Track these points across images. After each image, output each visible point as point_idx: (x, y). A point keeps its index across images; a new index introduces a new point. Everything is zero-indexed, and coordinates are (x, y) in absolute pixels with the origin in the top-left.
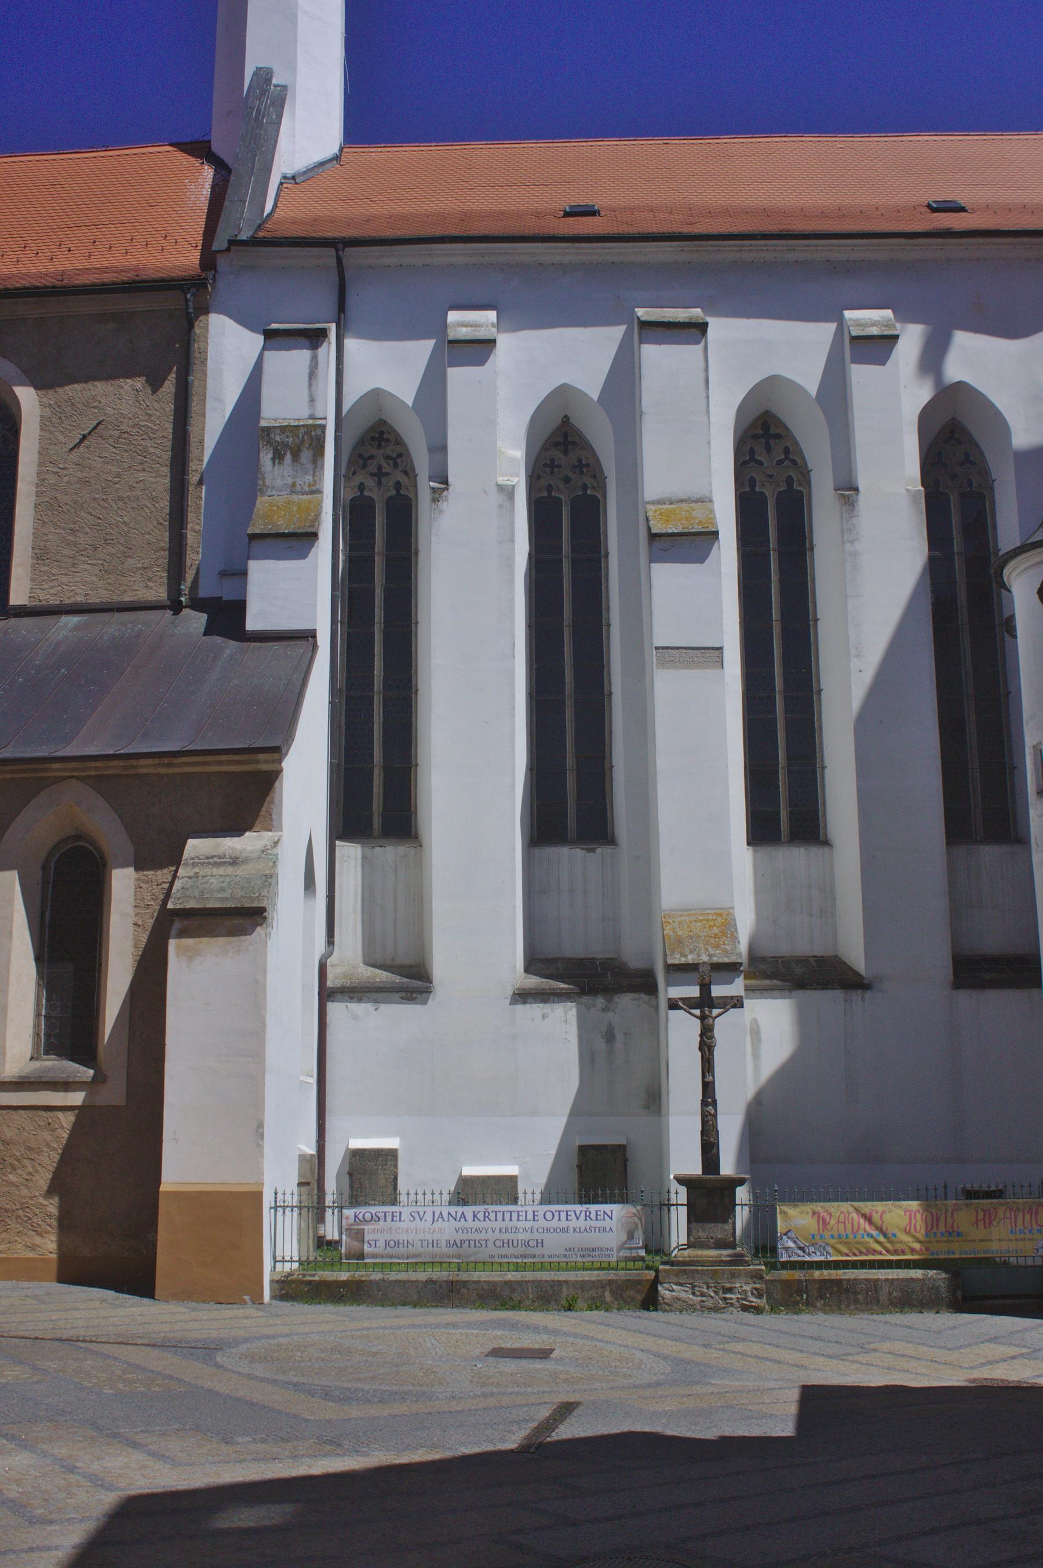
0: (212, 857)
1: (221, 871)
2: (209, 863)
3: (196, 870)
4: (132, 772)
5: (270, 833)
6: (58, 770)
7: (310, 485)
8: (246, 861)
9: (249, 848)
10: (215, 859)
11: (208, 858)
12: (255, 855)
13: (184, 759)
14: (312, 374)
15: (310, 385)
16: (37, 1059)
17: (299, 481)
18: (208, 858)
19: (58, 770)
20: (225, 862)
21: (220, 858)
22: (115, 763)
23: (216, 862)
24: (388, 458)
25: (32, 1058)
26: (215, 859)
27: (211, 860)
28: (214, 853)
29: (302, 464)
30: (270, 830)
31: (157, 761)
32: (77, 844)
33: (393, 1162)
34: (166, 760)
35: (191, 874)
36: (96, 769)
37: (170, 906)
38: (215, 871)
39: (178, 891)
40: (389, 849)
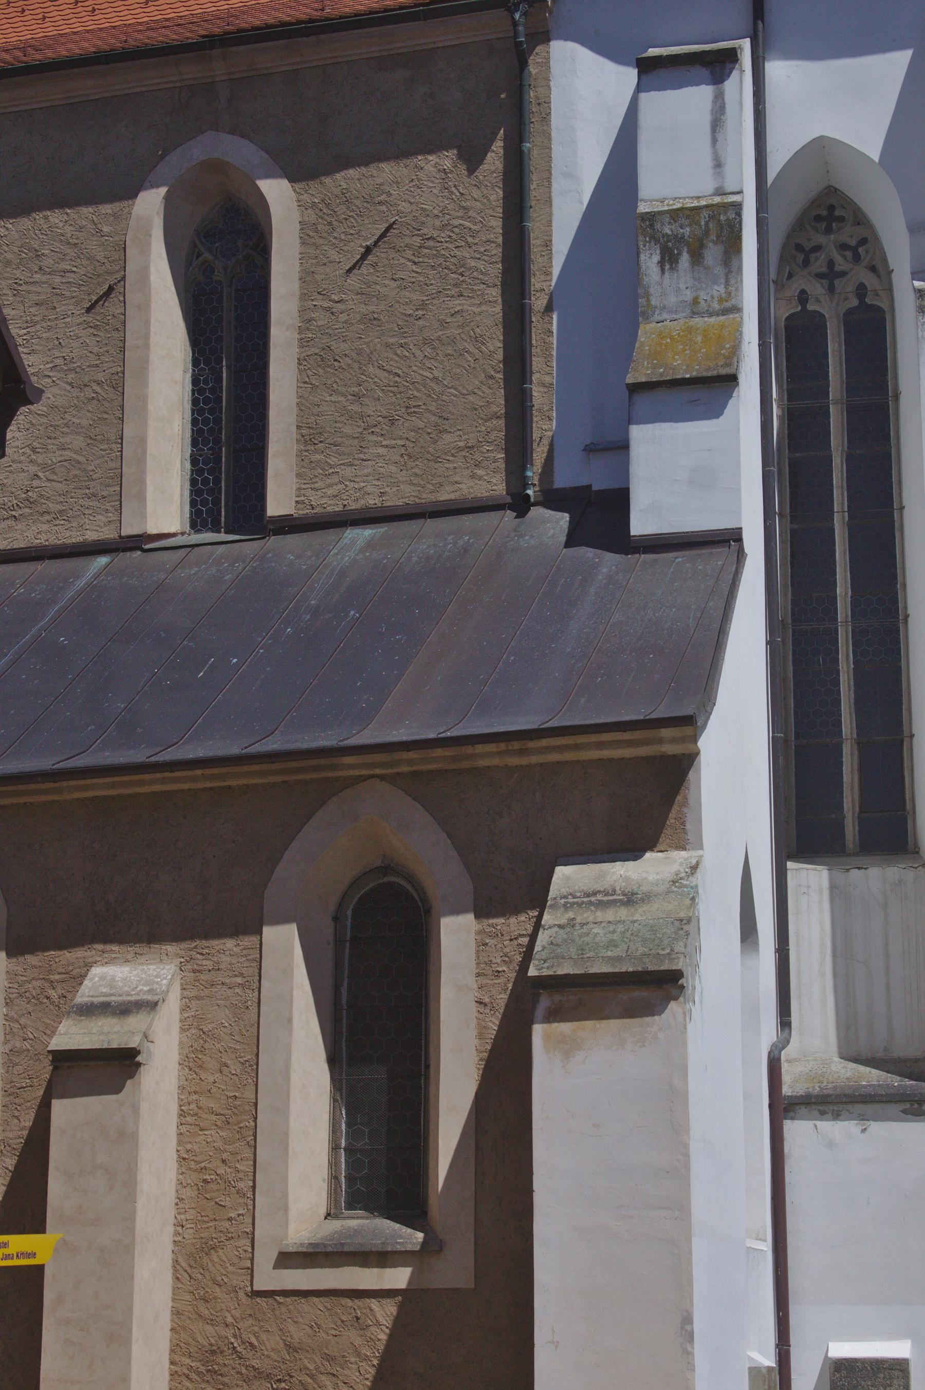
0: (595, 894)
1: (610, 915)
2: (591, 903)
3: (571, 915)
4: (466, 764)
5: (683, 854)
6: (352, 767)
7: (721, 300)
8: (647, 898)
9: (652, 877)
10: (599, 897)
11: (588, 895)
12: (662, 888)
13: (544, 742)
14: (717, 123)
15: (714, 141)
16: (336, 1217)
17: (703, 295)
18: (588, 895)
19: (352, 767)
20: (615, 901)
21: (607, 894)
22: (439, 752)
23: (601, 902)
24: (843, 247)
25: (328, 1216)
26: (599, 897)
27: (593, 899)
28: (597, 887)
29: (707, 268)
30: (685, 849)
31: (502, 746)
32: (386, 879)
33: (902, 1381)
34: (516, 745)
35: (563, 921)
36: (410, 762)
37: (532, 972)
38: (600, 915)
39: (544, 948)
40: (874, 872)
